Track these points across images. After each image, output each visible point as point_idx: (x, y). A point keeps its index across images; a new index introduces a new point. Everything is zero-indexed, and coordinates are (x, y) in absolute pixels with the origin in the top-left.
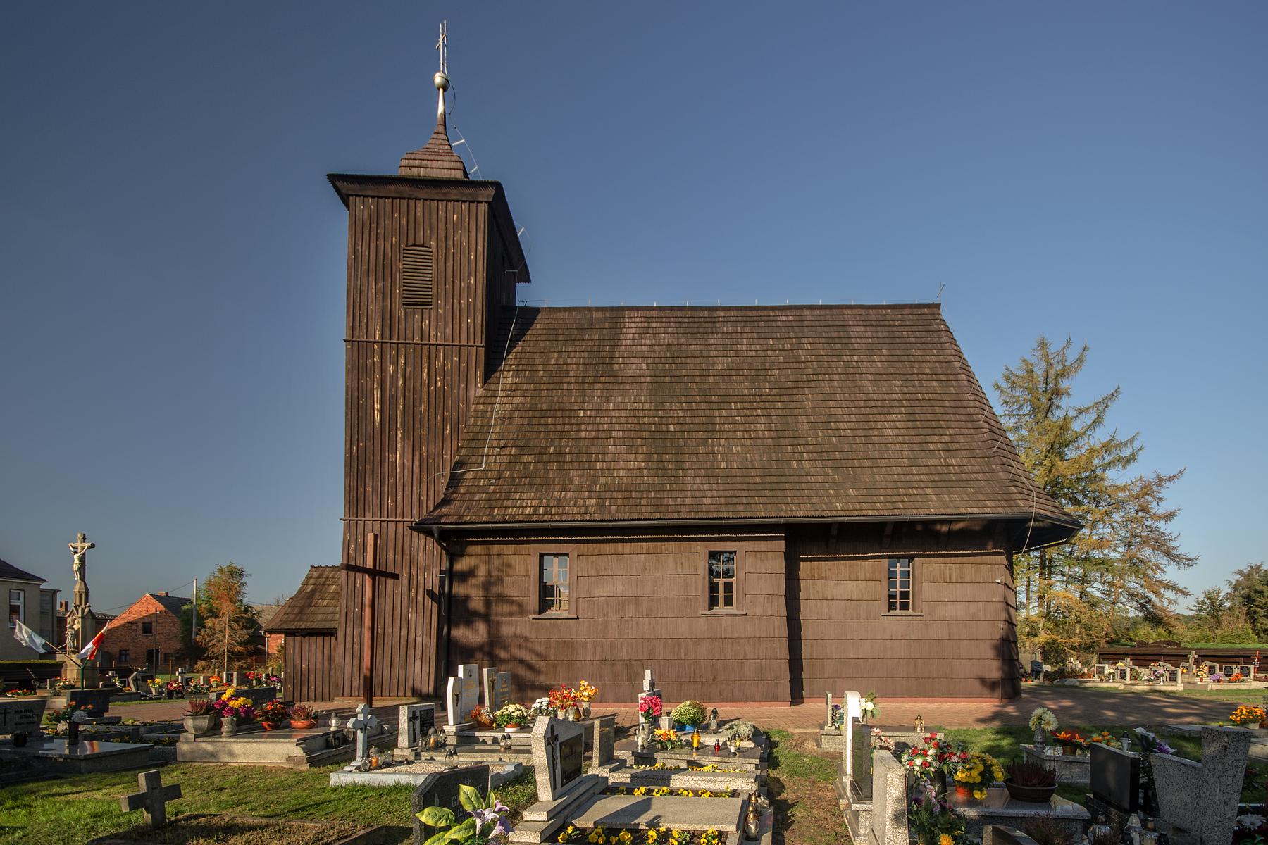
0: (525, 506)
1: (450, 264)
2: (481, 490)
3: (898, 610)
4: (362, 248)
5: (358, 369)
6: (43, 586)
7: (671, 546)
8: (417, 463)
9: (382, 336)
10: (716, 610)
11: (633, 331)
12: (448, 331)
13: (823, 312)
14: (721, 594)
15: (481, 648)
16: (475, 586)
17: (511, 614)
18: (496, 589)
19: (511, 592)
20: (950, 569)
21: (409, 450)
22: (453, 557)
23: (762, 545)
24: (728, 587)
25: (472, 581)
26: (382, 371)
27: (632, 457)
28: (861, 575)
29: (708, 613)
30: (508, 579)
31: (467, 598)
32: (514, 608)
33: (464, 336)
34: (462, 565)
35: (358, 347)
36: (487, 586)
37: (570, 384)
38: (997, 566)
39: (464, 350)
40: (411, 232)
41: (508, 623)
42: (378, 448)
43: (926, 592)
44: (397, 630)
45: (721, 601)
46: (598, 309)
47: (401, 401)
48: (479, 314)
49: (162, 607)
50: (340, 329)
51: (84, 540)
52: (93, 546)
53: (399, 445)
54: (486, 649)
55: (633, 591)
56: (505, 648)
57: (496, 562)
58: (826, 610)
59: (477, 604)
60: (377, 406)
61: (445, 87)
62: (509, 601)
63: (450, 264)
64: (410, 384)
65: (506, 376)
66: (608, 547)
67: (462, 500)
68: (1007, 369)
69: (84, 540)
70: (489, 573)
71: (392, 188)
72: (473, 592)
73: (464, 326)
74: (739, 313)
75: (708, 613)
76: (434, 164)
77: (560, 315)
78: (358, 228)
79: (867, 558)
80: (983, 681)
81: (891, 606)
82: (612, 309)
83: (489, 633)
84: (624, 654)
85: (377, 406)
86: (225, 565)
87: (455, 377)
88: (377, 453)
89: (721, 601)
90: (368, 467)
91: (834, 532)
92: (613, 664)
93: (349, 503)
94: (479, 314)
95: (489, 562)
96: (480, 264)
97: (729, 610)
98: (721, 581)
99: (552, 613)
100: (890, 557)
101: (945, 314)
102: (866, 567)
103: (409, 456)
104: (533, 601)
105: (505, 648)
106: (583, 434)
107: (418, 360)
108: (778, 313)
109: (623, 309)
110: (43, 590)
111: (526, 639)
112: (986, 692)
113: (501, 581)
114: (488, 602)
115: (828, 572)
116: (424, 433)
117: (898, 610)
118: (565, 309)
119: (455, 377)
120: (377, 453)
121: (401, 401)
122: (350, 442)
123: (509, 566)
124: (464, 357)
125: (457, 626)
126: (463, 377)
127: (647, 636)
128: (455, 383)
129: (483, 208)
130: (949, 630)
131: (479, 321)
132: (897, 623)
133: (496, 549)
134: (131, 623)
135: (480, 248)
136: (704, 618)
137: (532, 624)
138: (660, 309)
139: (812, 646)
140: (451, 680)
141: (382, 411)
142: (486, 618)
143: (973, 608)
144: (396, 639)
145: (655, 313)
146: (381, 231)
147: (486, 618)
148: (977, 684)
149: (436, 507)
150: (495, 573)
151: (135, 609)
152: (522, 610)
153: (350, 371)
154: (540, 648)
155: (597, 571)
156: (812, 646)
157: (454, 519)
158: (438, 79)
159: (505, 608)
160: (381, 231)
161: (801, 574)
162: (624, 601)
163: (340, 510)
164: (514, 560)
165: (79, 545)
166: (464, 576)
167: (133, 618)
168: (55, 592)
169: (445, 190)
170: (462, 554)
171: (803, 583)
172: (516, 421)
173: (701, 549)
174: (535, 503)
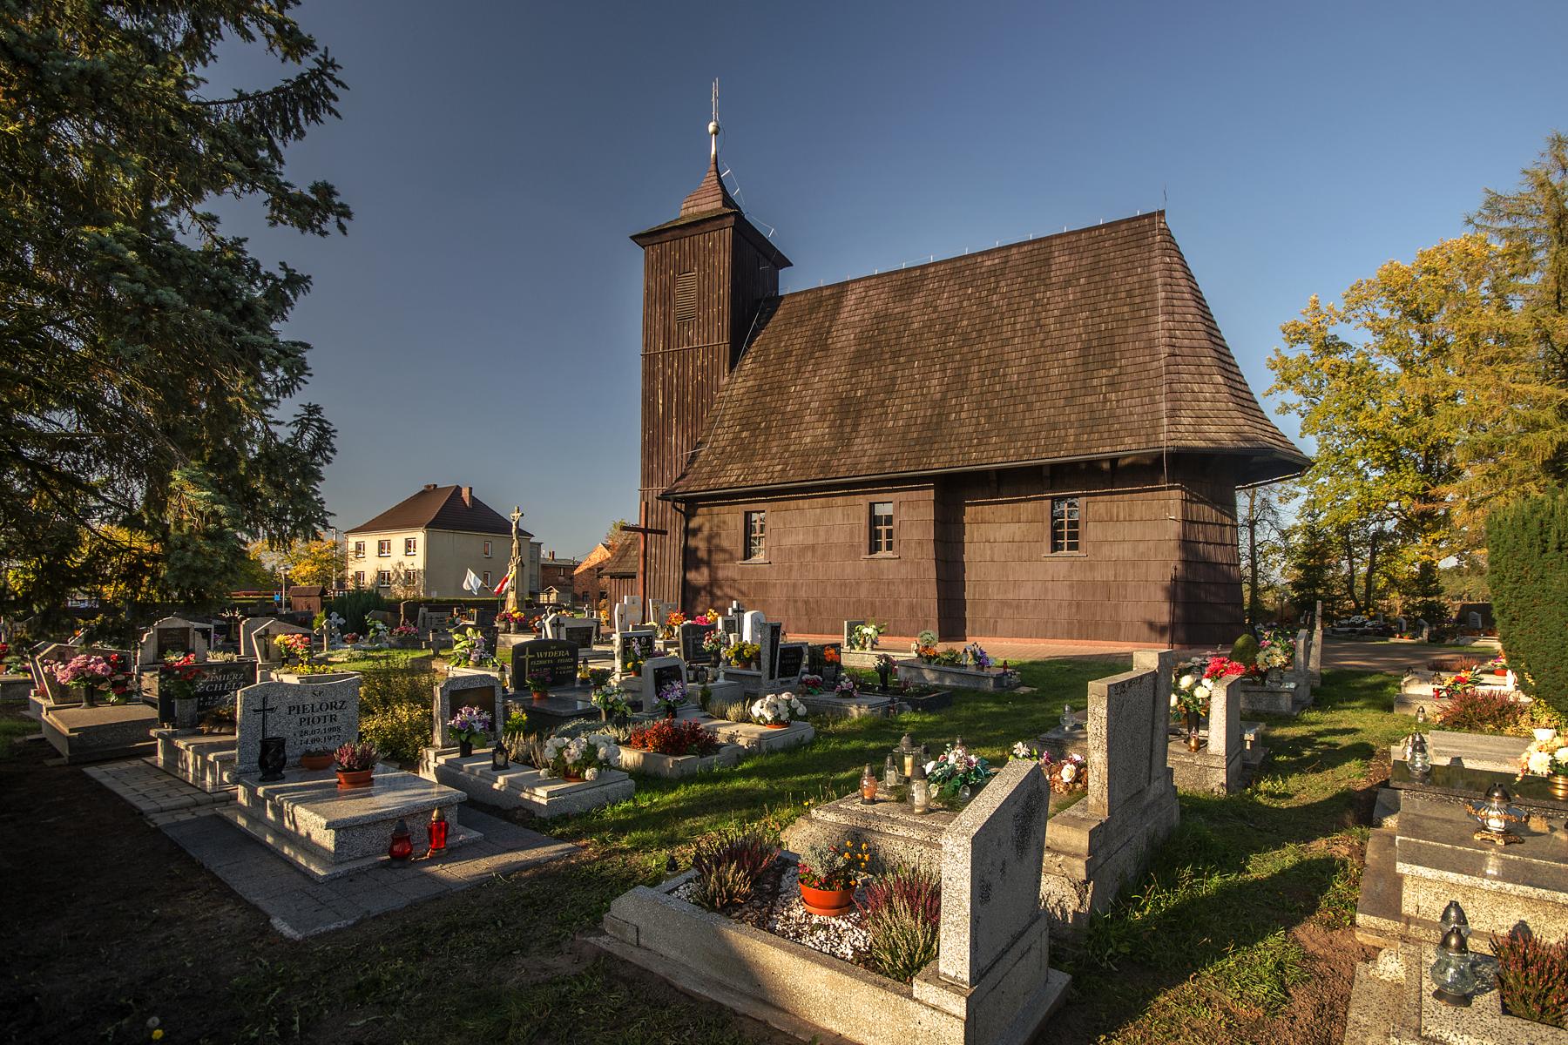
0: (733, 475)
1: (706, 282)
2: (708, 463)
3: (1065, 551)
4: (652, 284)
5: (649, 376)
6: (532, 540)
7: (840, 500)
8: (685, 442)
9: (663, 348)
10: (879, 554)
11: (852, 303)
12: (706, 335)
13: (1030, 248)
14: (884, 540)
15: (704, 588)
16: (701, 539)
17: (725, 561)
18: (715, 541)
19: (725, 544)
20: (1118, 507)
21: (680, 433)
22: (688, 516)
23: (914, 495)
24: (889, 534)
25: (700, 535)
26: (664, 374)
27: (820, 424)
28: (1023, 518)
29: (868, 557)
30: (723, 534)
31: (696, 549)
32: (727, 556)
33: (716, 337)
34: (693, 524)
35: (649, 359)
36: (710, 539)
37: (791, 364)
38: (1171, 502)
39: (716, 348)
40: (682, 263)
41: (723, 568)
42: (661, 433)
43: (1091, 533)
44: (672, 573)
45: (884, 546)
46: (827, 287)
47: (675, 395)
48: (726, 317)
49: (609, 555)
50: (640, 349)
51: (518, 511)
52: (522, 515)
53: (674, 430)
54: (708, 588)
55: (810, 541)
56: (720, 587)
57: (716, 520)
58: (989, 552)
59: (702, 554)
60: (661, 402)
61: (716, 133)
62: (724, 550)
63: (706, 282)
64: (681, 381)
65: (748, 364)
66: (792, 504)
67: (694, 473)
68: (1489, 192)
69: (518, 511)
70: (711, 529)
71: (669, 234)
72: (699, 543)
73: (716, 329)
74: (950, 266)
75: (868, 557)
76: (703, 201)
77: (798, 299)
78: (652, 269)
79: (1030, 500)
80: (1151, 625)
81: (1056, 547)
82: (839, 285)
83: (710, 576)
84: (803, 594)
85: (661, 402)
86: (618, 521)
87: (710, 371)
88: (661, 438)
89: (884, 546)
90: (655, 449)
91: (1046, 472)
92: (796, 601)
93: (643, 477)
94: (726, 317)
95: (710, 521)
96: (726, 278)
97: (889, 554)
98: (883, 528)
99: (754, 559)
100: (1053, 498)
101: (1171, 221)
102: (1027, 509)
103: (680, 437)
104: (740, 550)
105: (720, 587)
106: (789, 409)
107: (686, 362)
108: (985, 258)
109: (848, 283)
110: (532, 543)
111: (734, 580)
112: (1154, 636)
113: (718, 535)
114: (710, 552)
115: (991, 516)
116: (690, 418)
117: (1065, 551)
118: (801, 293)
119: (710, 371)
120: (661, 438)
121: (675, 395)
122: (644, 430)
123: (724, 522)
124: (716, 354)
125: (690, 570)
126: (715, 370)
127: (820, 577)
128: (710, 375)
129: (729, 231)
130: (1115, 570)
131: (725, 324)
132: (1060, 565)
133: (716, 509)
134: (590, 569)
135: (727, 265)
136: (865, 562)
137: (739, 569)
138: (879, 276)
139: (975, 587)
140: (617, 605)
141: (663, 404)
142: (708, 563)
143: (1142, 547)
144: (672, 580)
145: (873, 282)
146: (663, 268)
147: (708, 563)
148: (1145, 630)
149: (677, 480)
150: (715, 529)
151: (593, 556)
152: (732, 559)
153: (644, 378)
154: (744, 588)
155: (784, 524)
156: (975, 587)
157: (684, 489)
158: (711, 127)
159: (721, 556)
160: (663, 268)
161: (966, 519)
162: (804, 549)
163: (638, 483)
164: (728, 518)
165: (515, 515)
166: (695, 532)
167: (591, 564)
168: (540, 544)
169: (702, 226)
170: (694, 515)
171: (967, 527)
172: (745, 402)
173: (863, 501)
174: (739, 472)
